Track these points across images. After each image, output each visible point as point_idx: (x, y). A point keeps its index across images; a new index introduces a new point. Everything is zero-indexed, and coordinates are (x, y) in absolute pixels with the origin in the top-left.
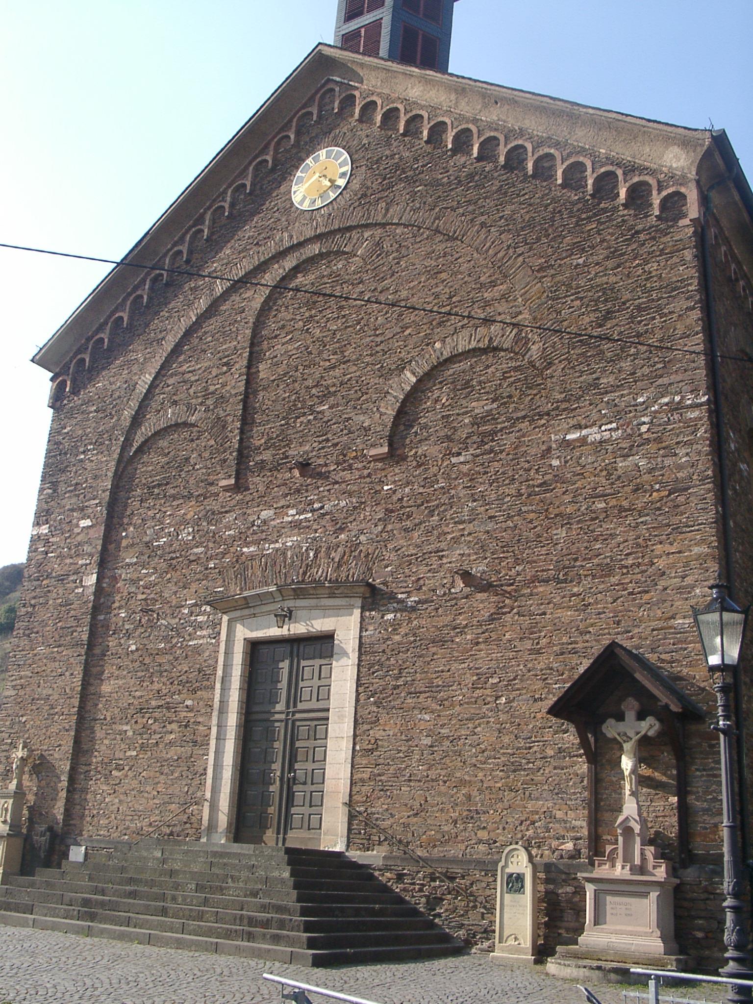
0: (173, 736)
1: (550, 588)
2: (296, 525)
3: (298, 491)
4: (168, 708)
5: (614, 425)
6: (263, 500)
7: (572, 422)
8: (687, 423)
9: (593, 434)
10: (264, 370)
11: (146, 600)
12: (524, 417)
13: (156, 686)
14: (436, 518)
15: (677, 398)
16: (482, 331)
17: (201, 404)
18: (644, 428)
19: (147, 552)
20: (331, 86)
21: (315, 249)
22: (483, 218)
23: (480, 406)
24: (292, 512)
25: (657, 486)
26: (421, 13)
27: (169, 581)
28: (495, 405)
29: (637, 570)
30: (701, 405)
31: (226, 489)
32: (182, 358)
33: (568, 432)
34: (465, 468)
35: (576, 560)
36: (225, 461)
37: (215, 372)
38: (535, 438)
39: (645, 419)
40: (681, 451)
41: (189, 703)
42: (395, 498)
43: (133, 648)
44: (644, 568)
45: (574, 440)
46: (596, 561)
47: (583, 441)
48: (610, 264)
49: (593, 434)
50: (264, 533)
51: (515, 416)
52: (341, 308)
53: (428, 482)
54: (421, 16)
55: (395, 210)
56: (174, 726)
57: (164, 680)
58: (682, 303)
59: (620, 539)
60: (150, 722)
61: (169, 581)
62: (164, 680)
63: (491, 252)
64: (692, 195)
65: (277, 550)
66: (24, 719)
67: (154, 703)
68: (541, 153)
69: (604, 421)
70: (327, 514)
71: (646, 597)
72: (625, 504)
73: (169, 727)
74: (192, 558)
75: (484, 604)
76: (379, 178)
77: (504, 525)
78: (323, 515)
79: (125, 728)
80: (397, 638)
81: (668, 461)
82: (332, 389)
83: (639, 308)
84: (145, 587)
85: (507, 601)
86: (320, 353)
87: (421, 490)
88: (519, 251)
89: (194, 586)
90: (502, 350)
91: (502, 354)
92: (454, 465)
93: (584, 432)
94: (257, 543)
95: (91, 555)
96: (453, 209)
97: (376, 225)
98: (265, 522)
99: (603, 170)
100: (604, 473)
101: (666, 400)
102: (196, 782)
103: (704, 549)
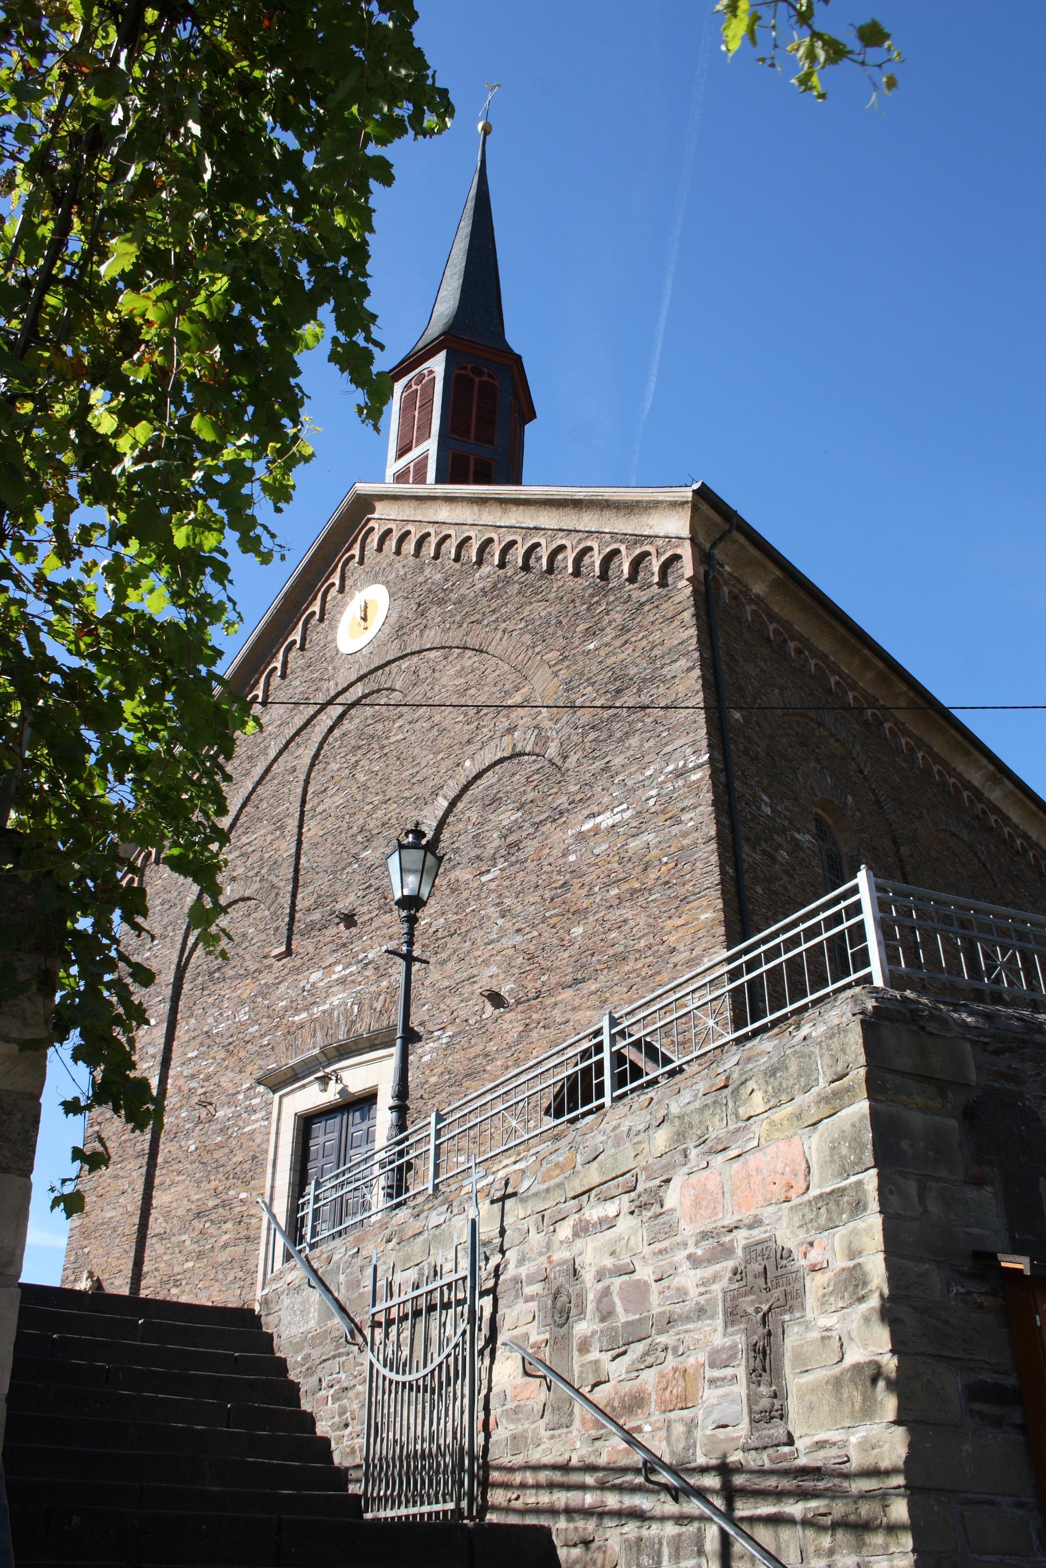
0: (227, 1236)
1: (568, 993)
2: (342, 981)
3: (344, 945)
4: (224, 1206)
5: (625, 806)
6: (312, 962)
7: (586, 812)
8: (690, 786)
9: (606, 820)
10: (312, 830)
11: (205, 1093)
12: (546, 820)
13: (214, 1184)
14: (468, 943)
15: (681, 764)
16: (507, 739)
17: (256, 875)
18: (652, 802)
19: (207, 1041)
20: (371, 524)
21: (358, 691)
22: (504, 625)
23: (508, 816)
24: (339, 968)
25: (665, 860)
26: (472, 436)
27: (226, 1068)
28: (520, 814)
29: (650, 952)
30: (703, 765)
31: (279, 957)
32: (240, 831)
33: (583, 823)
34: (493, 886)
35: (593, 955)
36: (277, 929)
37: (269, 838)
38: (561, 836)
39: (654, 792)
40: (685, 817)
41: (243, 1195)
42: (431, 931)
43: (193, 1148)
44: (655, 948)
45: (589, 831)
46: (611, 952)
47: (596, 831)
48: (618, 643)
49: (606, 820)
50: (313, 996)
51: (538, 820)
52: (383, 747)
53: (460, 908)
54: (472, 440)
55: (430, 634)
56: (229, 1225)
57: (220, 1176)
58: (683, 663)
59: (632, 923)
60: (208, 1225)
61: (226, 1068)
62: (220, 1176)
63: (513, 657)
64: (686, 551)
65: (324, 1012)
66: (86, 1250)
67: (211, 1204)
68: (554, 546)
69: (616, 803)
70: (370, 963)
71: (658, 978)
72: (637, 885)
73: (225, 1227)
74: (247, 1038)
75: (511, 1022)
76: (418, 604)
77: (529, 936)
78: (367, 964)
79: (184, 1237)
80: (433, 1080)
81: (676, 829)
82: (375, 832)
83: (644, 681)
84: (204, 1080)
85: (534, 1016)
86: (365, 796)
87: (455, 917)
88: (537, 650)
89: (249, 1069)
90: (525, 754)
91: (526, 758)
92: (483, 885)
93: (598, 819)
94: (306, 1009)
95: (154, 1057)
96: (478, 622)
97: (413, 653)
98: (313, 985)
99: (608, 550)
100: (617, 858)
101: (670, 768)
102: (249, 1281)
103: (707, 916)
